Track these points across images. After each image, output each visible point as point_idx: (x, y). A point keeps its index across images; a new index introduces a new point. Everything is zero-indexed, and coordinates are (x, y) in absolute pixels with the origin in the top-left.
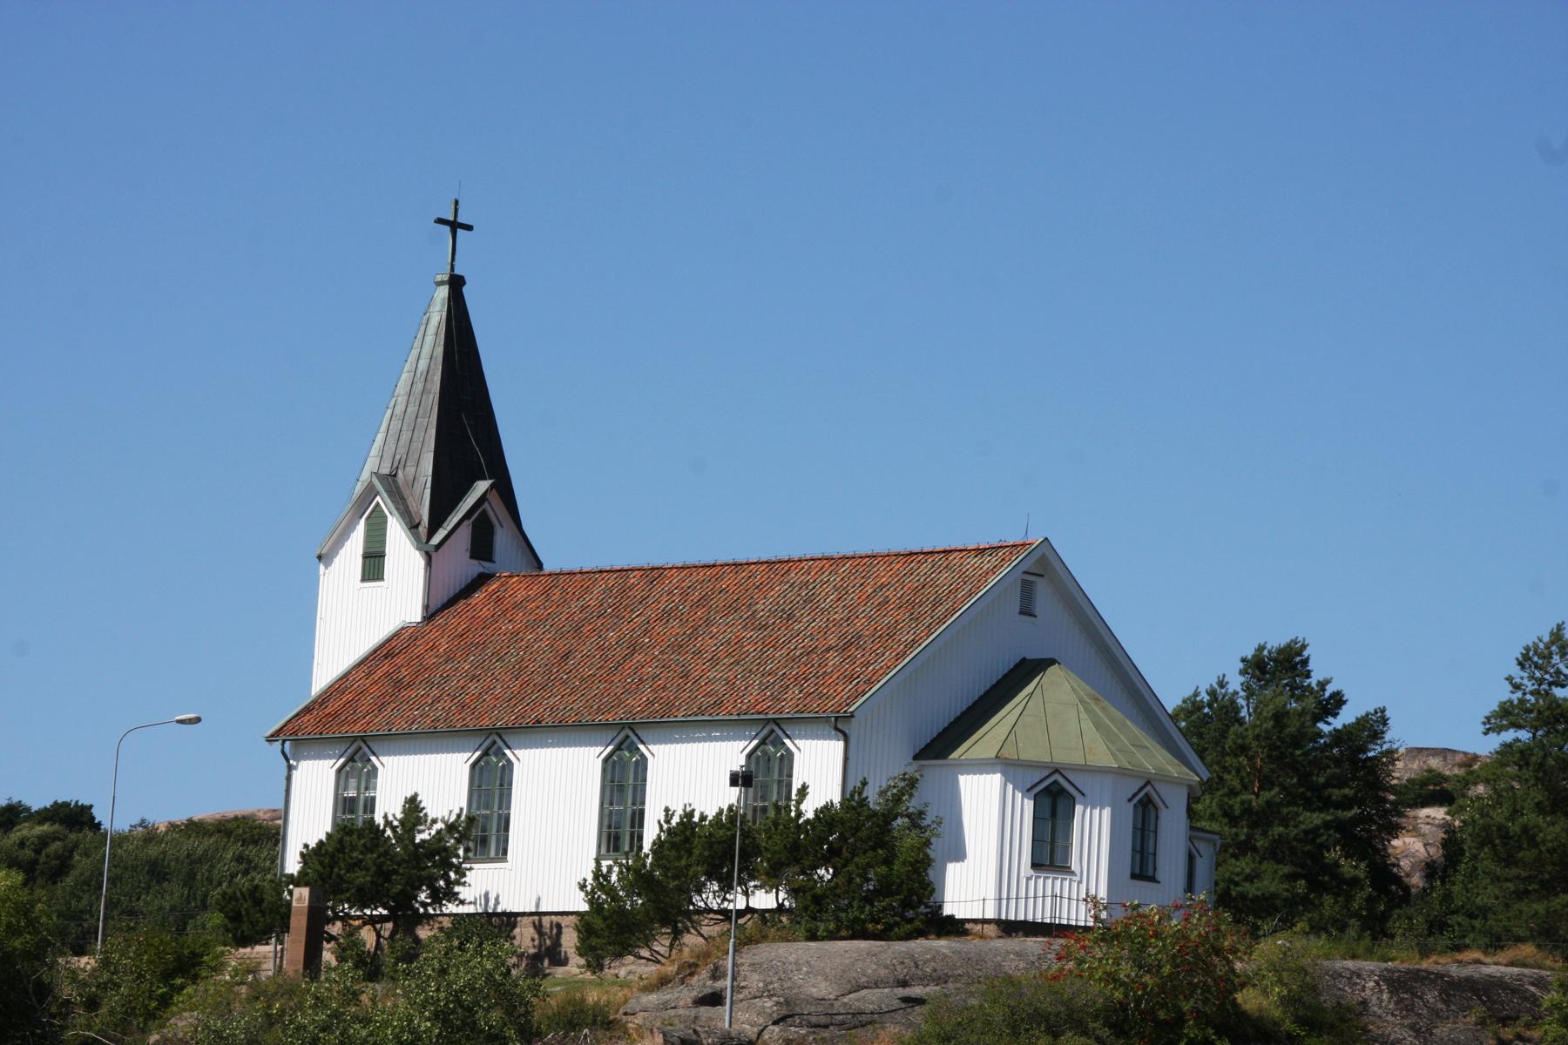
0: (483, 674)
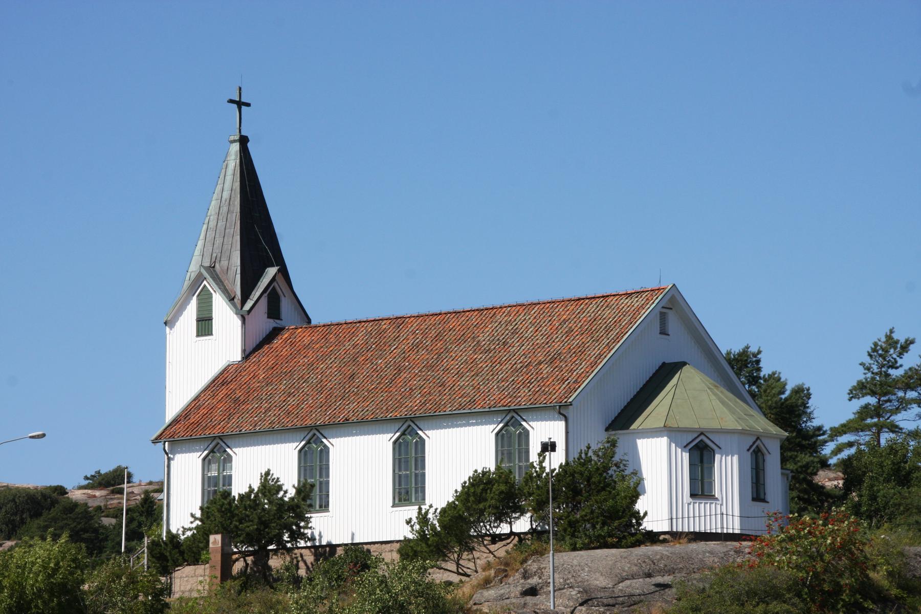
0: (296, 392)
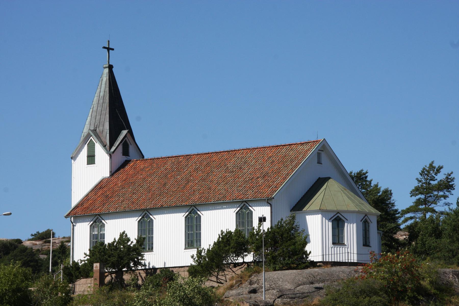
0: (137, 192)
